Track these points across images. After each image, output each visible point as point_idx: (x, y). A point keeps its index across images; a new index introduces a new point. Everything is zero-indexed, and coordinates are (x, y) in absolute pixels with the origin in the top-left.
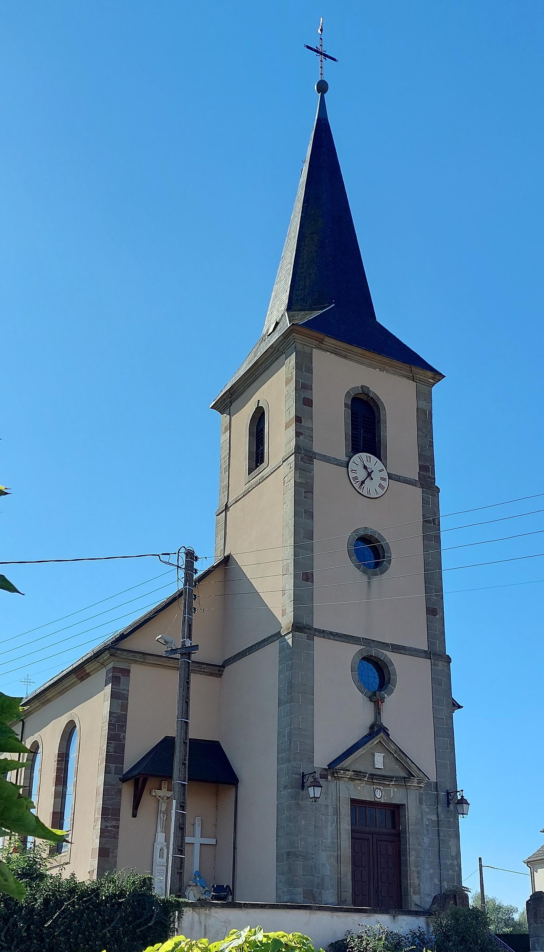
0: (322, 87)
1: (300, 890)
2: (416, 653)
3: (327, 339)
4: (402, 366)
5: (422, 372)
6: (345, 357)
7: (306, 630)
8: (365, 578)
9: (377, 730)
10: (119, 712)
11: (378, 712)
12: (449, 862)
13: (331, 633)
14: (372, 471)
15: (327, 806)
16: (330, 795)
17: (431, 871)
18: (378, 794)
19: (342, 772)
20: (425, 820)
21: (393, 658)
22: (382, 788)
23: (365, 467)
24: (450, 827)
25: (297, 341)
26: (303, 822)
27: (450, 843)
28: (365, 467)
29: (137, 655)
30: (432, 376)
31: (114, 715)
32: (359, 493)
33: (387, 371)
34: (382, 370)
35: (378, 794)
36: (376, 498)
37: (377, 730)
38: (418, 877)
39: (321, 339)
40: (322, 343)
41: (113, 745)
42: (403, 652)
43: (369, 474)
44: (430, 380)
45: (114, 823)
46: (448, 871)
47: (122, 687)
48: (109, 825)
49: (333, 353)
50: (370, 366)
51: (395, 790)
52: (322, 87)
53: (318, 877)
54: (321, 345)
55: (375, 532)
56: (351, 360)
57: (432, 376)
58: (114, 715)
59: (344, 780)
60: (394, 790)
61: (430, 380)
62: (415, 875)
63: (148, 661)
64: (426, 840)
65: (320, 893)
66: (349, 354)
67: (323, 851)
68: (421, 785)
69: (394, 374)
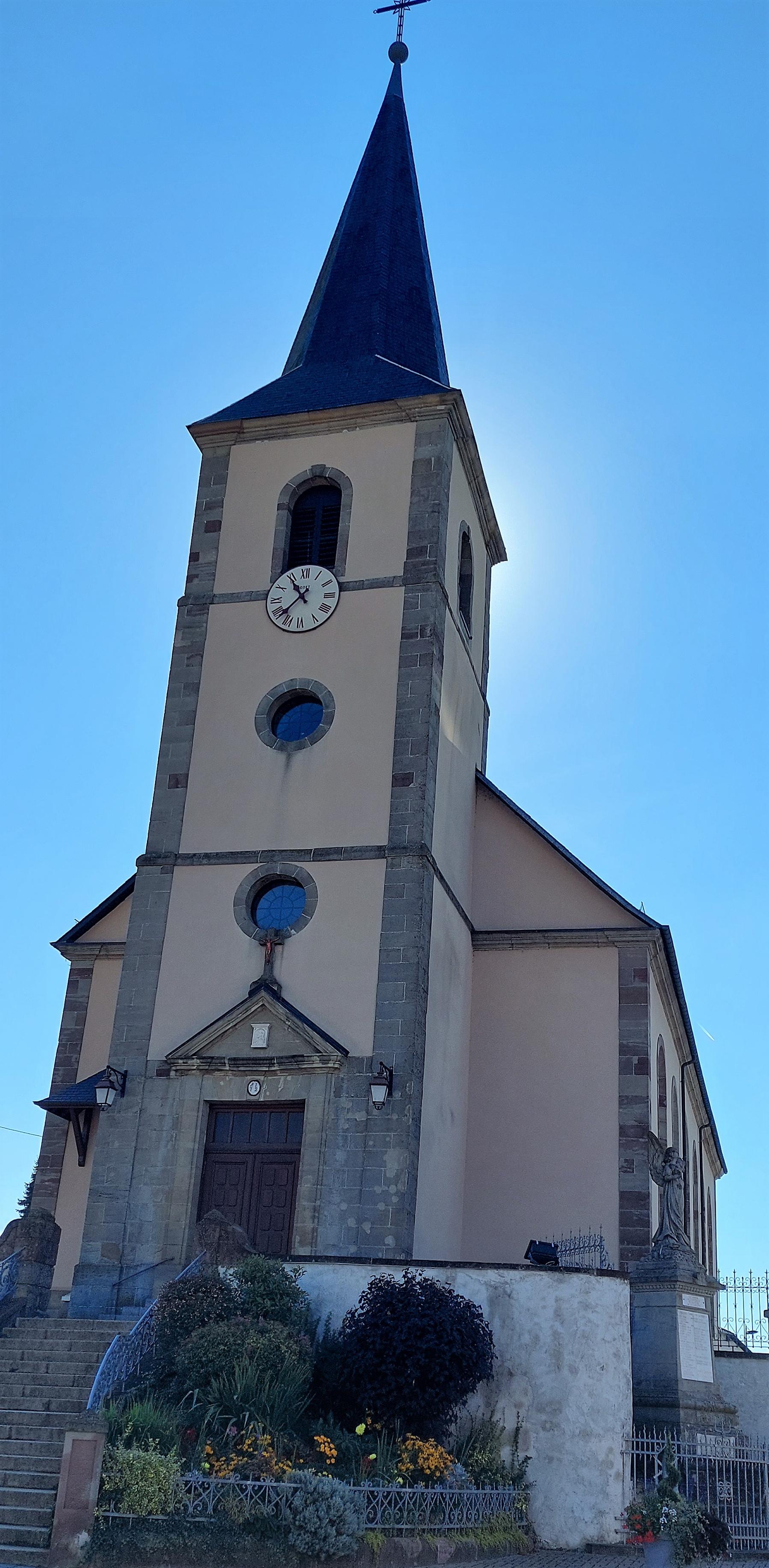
0: (398, 53)
1: (98, 1244)
2: (360, 853)
3: (246, 424)
4: (383, 408)
5: (416, 401)
6: (286, 436)
7: (160, 861)
8: (281, 757)
9: (266, 986)
10: (73, 1027)
11: (269, 962)
12: (378, 1189)
13: (207, 856)
14: (307, 590)
15: (162, 1116)
16: (170, 1101)
17: (344, 1206)
18: (254, 1089)
19: (181, 1061)
20: (342, 1121)
21: (311, 868)
22: (262, 1078)
23: (296, 588)
24: (388, 1130)
25: (206, 446)
26: (117, 1144)
27: (385, 1158)
28: (296, 588)
29: (94, 947)
30: (438, 399)
31: (66, 1032)
32: (284, 630)
33: (362, 427)
34: (351, 428)
35: (254, 1089)
36: (315, 629)
37: (266, 986)
38: (314, 1217)
39: (237, 427)
40: (243, 433)
41: (61, 1073)
42: (335, 857)
43: (302, 597)
44: (439, 408)
45: (53, 1176)
46: (376, 1204)
47: (80, 994)
48: (46, 1178)
49: (266, 439)
50: (329, 431)
51: (289, 1078)
52: (398, 53)
53: (132, 1225)
54: (242, 435)
55: (309, 682)
56: (297, 435)
57: (438, 399)
58: (66, 1032)
59: (193, 1074)
60: (285, 1080)
61: (439, 408)
62: (308, 1214)
63: (113, 953)
64: (340, 1156)
65: (133, 1249)
66: (290, 429)
67: (145, 1184)
68: (329, 1065)
69: (375, 425)
